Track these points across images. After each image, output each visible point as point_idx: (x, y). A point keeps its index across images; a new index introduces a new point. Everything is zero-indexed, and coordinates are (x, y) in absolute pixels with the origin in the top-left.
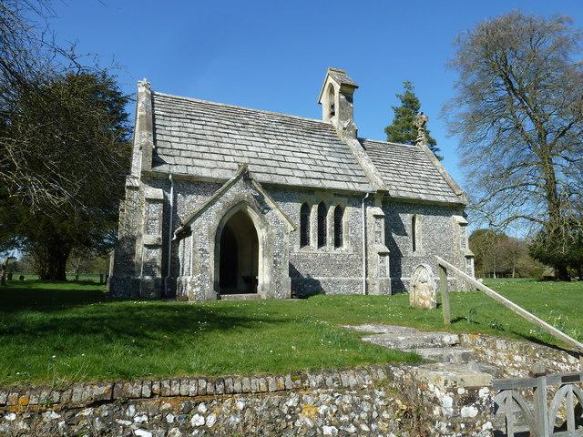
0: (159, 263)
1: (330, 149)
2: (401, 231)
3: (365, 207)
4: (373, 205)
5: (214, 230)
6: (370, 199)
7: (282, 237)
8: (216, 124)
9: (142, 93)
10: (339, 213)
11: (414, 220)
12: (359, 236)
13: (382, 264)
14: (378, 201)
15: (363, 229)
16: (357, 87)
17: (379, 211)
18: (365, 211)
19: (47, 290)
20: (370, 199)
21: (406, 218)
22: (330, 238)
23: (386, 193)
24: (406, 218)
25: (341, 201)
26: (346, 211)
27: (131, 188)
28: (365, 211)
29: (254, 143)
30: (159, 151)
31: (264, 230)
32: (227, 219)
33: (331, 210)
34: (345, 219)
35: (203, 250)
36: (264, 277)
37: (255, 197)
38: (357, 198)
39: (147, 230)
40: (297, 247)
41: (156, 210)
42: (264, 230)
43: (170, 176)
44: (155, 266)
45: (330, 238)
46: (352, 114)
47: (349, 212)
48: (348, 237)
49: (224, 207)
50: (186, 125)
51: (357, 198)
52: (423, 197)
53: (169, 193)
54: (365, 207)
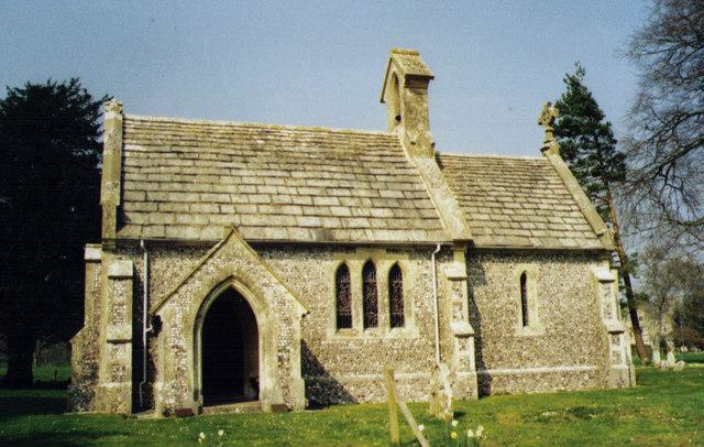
1: (388, 178)
8: (214, 157)
9: (110, 120)
12: (429, 310)
13: (463, 352)
16: (432, 78)
22: (383, 316)
27: (91, 261)
29: (268, 181)
30: (127, 206)
36: (267, 381)
43: (142, 244)
45: (383, 316)
46: (426, 120)
50: (171, 162)
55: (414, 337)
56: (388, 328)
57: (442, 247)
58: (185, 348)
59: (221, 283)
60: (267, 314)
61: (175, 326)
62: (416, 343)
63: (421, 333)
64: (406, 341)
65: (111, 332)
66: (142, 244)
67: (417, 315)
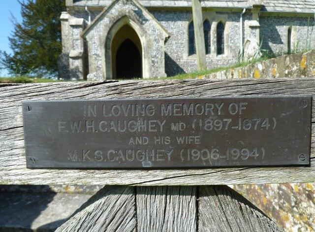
0: (81, 69)
2: (277, 39)
3: (244, 20)
4: (250, 19)
5: (104, 39)
6: (248, 14)
7: (158, 42)
10: (221, 27)
11: (289, 31)
12: (238, 45)
14: (255, 15)
15: (241, 39)
17: (255, 23)
18: (243, 24)
19: (60, 104)
20: (248, 14)
21: (282, 30)
22: (213, 47)
23: (262, 8)
24: (282, 30)
25: (222, 17)
26: (226, 24)
28: (243, 24)
31: (144, 37)
32: (114, 31)
33: (214, 26)
34: (226, 32)
35: (96, 55)
37: (135, 11)
38: (235, 14)
39: (73, 48)
40: (185, 55)
41: (77, 32)
42: (144, 37)
43: (86, 8)
44: (79, 71)
45: (213, 47)
47: (229, 26)
48: (228, 46)
49: (110, 21)
51: (235, 14)
52: (299, 11)
53: (88, 21)
54: (244, 20)
55: (229, 58)
56: (215, 54)
57: (246, 10)
58: (100, 55)
59: (119, 20)
60: (146, 37)
61: (95, 43)
62: (230, 62)
63: (233, 57)
64: (225, 60)
65: (73, 53)
66: (86, 8)
67: (231, 47)
